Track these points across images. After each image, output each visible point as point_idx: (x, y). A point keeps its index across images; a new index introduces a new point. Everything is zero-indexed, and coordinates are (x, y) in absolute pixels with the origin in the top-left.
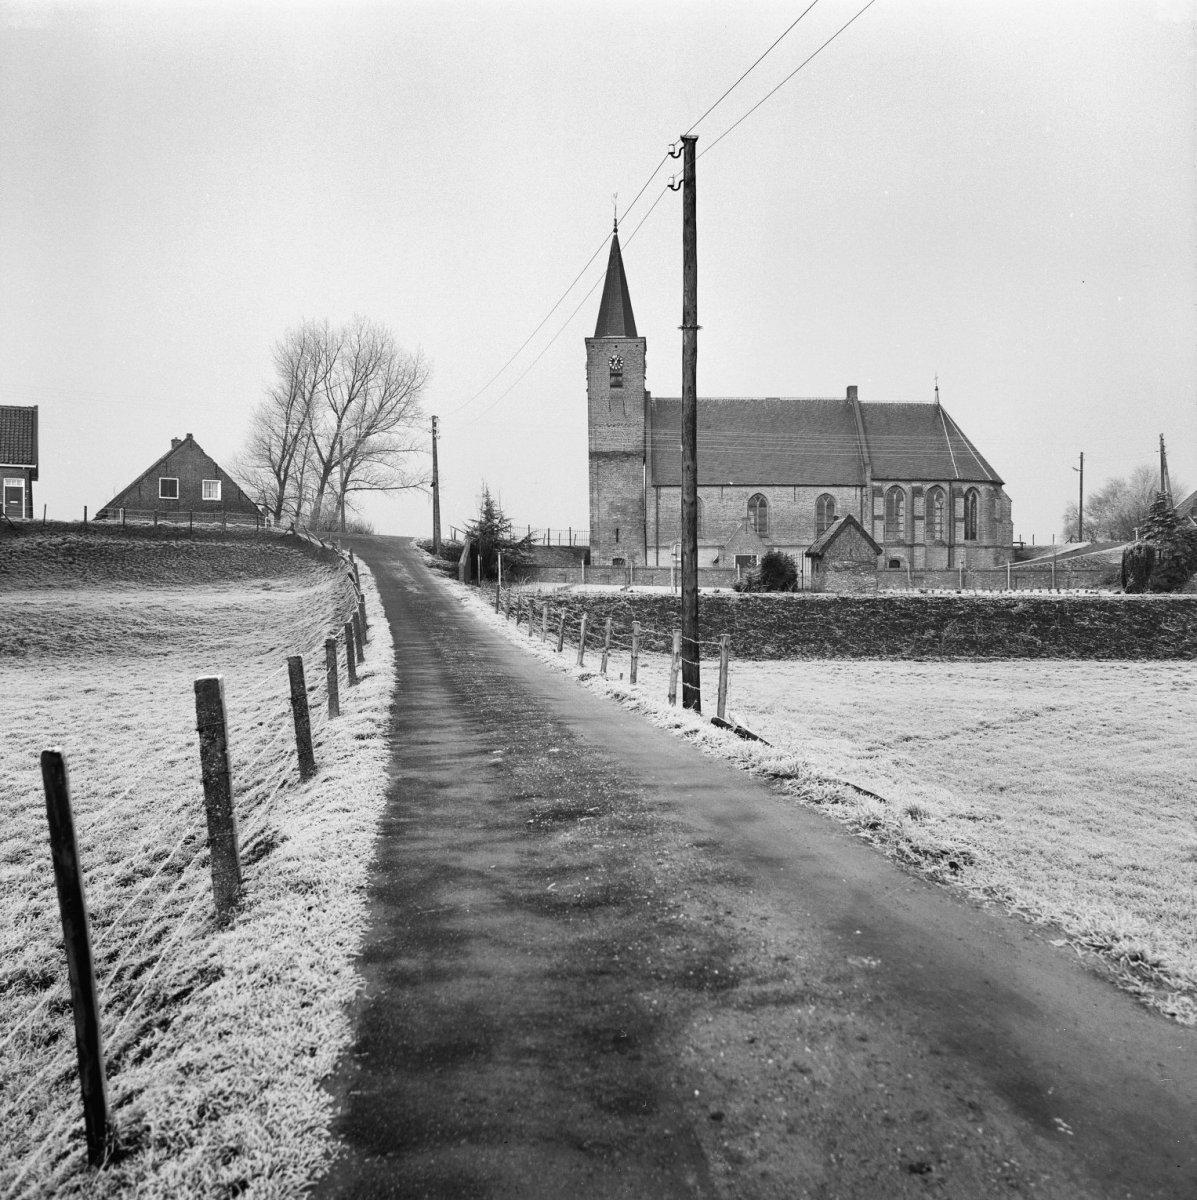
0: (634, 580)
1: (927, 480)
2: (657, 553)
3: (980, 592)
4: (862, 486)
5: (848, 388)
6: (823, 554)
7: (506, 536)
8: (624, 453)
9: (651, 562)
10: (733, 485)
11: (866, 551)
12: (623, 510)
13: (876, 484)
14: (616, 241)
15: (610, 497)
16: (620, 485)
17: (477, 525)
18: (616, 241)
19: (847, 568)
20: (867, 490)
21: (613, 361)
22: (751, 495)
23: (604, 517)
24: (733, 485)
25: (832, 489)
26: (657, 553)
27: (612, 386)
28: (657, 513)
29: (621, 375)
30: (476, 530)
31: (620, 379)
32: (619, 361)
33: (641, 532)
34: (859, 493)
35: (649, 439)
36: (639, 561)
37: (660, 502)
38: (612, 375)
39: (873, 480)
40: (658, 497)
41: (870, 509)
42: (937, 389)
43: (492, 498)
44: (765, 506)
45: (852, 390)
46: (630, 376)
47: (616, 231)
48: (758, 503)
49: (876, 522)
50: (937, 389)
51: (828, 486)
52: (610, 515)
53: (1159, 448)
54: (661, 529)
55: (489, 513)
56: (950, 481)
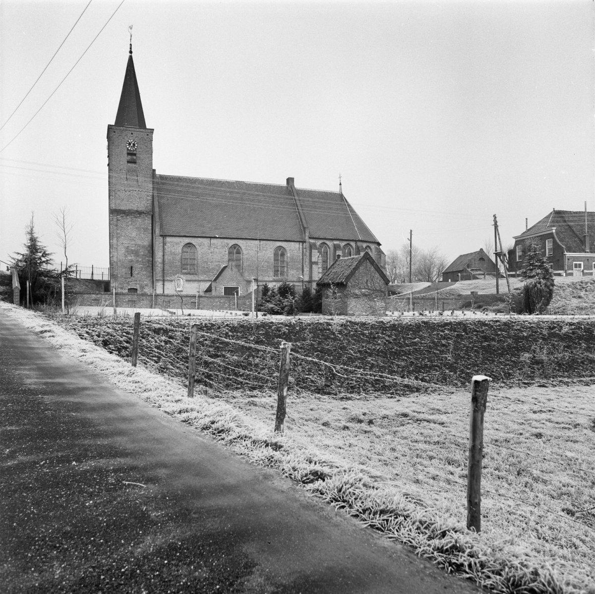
0: (156, 304)
1: (342, 240)
2: (163, 284)
3: (109, 311)
4: (303, 242)
5: (287, 179)
6: (346, 284)
7: (45, 267)
8: (137, 211)
9: (159, 291)
10: (218, 238)
11: (379, 282)
12: (136, 253)
13: (312, 241)
14: (131, 60)
15: (126, 242)
16: (134, 234)
17: (20, 257)
18: (131, 60)
19: (365, 295)
20: (306, 245)
21: (130, 144)
22: (230, 245)
23: (122, 258)
24: (218, 238)
25: (284, 243)
26: (163, 284)
27: (128, 162)
28: (163, 255)
29: (135, 155)
30: (21, 261)
31: (135, 157)
32: (134, 144)
33: (149, 269)
34: (301, 246)
35: (156, 203)
36: (148, 290)
37: (165, 247)
38: (128, 154)
39: (310, 238)
40: (164, 244)
41: (308, 257)
42: (340, 184)
43: (35, 235)
44: (240, 253)
45: (290, 181)
46: (141, 156)
47: (131, 52)
48: (236, 250)
49: (313, 266)
50: (340, 184)
51: (281, 241)
52: (126, 256)
53: (493, 223)
54: (167, 267)
55: (33, 247)
56: (356, 241)
